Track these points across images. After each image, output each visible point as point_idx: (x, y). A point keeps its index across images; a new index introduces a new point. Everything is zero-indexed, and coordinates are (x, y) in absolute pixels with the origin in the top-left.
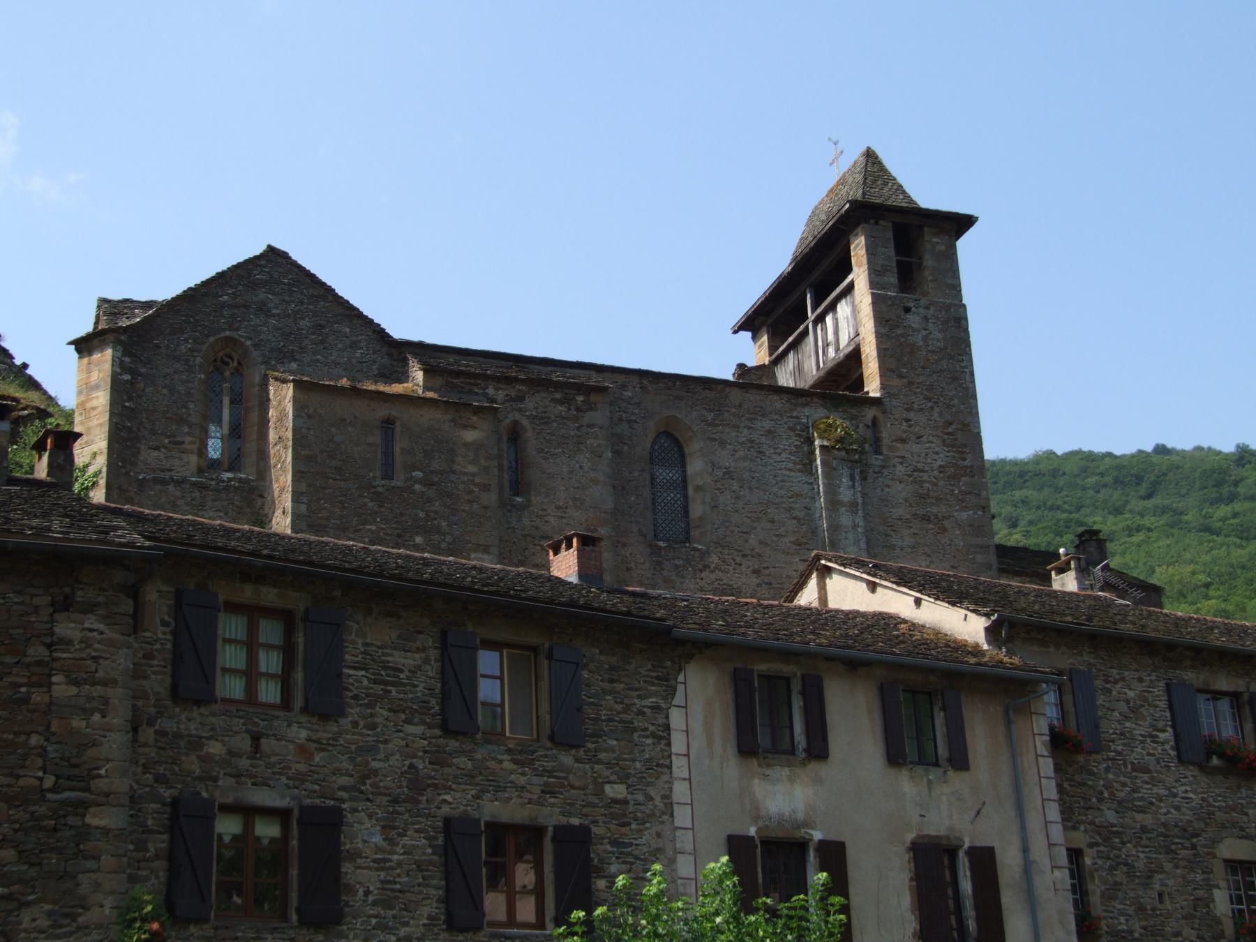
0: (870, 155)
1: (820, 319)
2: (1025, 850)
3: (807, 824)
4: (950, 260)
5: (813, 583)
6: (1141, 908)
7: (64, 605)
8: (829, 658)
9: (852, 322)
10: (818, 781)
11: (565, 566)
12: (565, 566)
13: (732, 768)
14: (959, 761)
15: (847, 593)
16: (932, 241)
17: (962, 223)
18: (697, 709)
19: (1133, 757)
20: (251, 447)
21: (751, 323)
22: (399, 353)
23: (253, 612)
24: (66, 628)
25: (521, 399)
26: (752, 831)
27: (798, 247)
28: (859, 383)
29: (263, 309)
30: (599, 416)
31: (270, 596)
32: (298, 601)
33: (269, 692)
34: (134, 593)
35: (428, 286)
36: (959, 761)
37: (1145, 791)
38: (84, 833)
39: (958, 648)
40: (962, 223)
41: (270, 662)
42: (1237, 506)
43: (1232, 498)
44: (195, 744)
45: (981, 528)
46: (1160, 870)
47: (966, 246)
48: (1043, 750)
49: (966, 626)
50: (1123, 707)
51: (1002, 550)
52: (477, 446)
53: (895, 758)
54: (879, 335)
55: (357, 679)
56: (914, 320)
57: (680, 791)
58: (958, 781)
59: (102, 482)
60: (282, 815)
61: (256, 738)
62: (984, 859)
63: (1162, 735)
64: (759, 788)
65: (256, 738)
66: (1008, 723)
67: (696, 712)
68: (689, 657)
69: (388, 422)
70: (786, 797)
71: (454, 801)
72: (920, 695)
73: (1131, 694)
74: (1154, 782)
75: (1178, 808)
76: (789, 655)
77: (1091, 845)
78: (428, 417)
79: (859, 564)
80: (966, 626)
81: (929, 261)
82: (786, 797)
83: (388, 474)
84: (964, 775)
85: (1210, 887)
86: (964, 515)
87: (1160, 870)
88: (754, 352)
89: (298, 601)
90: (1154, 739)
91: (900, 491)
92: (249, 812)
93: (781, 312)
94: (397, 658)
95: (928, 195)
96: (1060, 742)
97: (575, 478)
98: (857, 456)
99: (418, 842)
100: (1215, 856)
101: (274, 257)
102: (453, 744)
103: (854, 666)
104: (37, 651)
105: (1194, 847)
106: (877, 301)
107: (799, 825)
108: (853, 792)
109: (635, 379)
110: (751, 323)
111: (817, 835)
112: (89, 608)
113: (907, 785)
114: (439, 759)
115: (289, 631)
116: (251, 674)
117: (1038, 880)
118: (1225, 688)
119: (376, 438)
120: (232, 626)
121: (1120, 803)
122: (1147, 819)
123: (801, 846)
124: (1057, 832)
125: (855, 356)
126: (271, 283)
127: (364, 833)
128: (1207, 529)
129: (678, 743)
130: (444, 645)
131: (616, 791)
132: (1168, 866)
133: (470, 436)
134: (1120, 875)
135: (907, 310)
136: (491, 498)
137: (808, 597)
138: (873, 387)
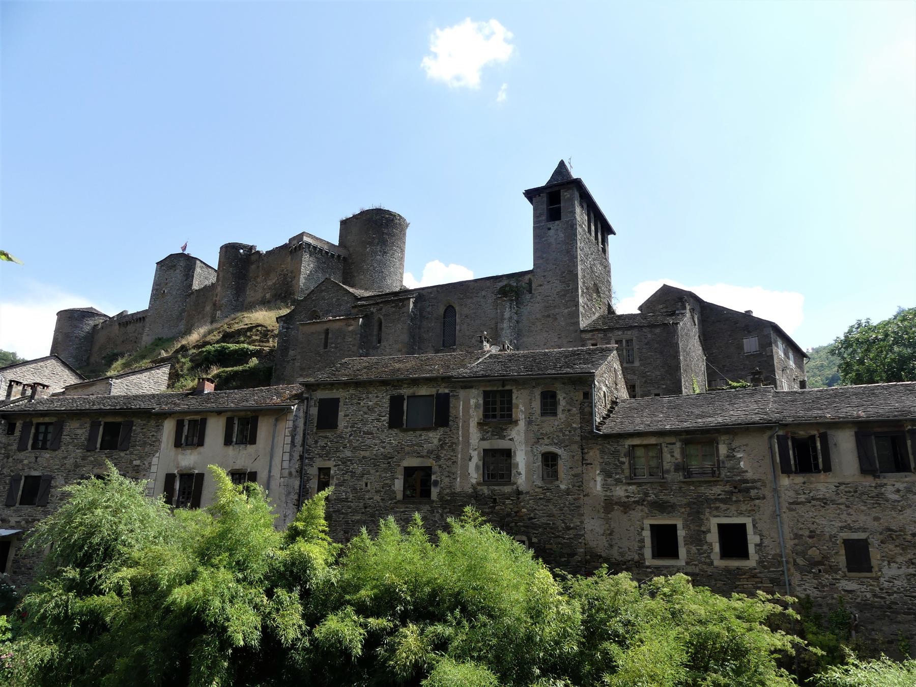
2: (270, 472)
3: (194, 468)
6: (355, 489)
10: (200, 453)
19: (365, 429)
25: (381, 309)
26: (176, 472)
29: (324, 299)
37: (368, 442)
44: (21, 461)
48: (287, 433)
50: (365, 409)
55: (66, 438)
56: (552, 232)
58: (251, 448)
61: (37, 458)
63: (383, 418)
64: (180, 457)
65: (37, 458)
66: (275, 425)
68: (166, 418)
70: (189, 460)
73: (370, 403)
74: (374, 438)
75: (384, 448)
77: (335, 466)
82: (189, 460)
84: (254, 446)
85: (393, 478)
86: (566, 311)
90: (378, 420)
100: (399, 466)
102: (89, 453)
105: (389, 463)
107: (191, 469)
109: (488, 283)
111: (196, 472)
118: (424, 394)
121: (354, 448)
122: (367, 454)
124: (286, 464)
132: (372, 471)
134: (347, 477)
135: (549, 229)
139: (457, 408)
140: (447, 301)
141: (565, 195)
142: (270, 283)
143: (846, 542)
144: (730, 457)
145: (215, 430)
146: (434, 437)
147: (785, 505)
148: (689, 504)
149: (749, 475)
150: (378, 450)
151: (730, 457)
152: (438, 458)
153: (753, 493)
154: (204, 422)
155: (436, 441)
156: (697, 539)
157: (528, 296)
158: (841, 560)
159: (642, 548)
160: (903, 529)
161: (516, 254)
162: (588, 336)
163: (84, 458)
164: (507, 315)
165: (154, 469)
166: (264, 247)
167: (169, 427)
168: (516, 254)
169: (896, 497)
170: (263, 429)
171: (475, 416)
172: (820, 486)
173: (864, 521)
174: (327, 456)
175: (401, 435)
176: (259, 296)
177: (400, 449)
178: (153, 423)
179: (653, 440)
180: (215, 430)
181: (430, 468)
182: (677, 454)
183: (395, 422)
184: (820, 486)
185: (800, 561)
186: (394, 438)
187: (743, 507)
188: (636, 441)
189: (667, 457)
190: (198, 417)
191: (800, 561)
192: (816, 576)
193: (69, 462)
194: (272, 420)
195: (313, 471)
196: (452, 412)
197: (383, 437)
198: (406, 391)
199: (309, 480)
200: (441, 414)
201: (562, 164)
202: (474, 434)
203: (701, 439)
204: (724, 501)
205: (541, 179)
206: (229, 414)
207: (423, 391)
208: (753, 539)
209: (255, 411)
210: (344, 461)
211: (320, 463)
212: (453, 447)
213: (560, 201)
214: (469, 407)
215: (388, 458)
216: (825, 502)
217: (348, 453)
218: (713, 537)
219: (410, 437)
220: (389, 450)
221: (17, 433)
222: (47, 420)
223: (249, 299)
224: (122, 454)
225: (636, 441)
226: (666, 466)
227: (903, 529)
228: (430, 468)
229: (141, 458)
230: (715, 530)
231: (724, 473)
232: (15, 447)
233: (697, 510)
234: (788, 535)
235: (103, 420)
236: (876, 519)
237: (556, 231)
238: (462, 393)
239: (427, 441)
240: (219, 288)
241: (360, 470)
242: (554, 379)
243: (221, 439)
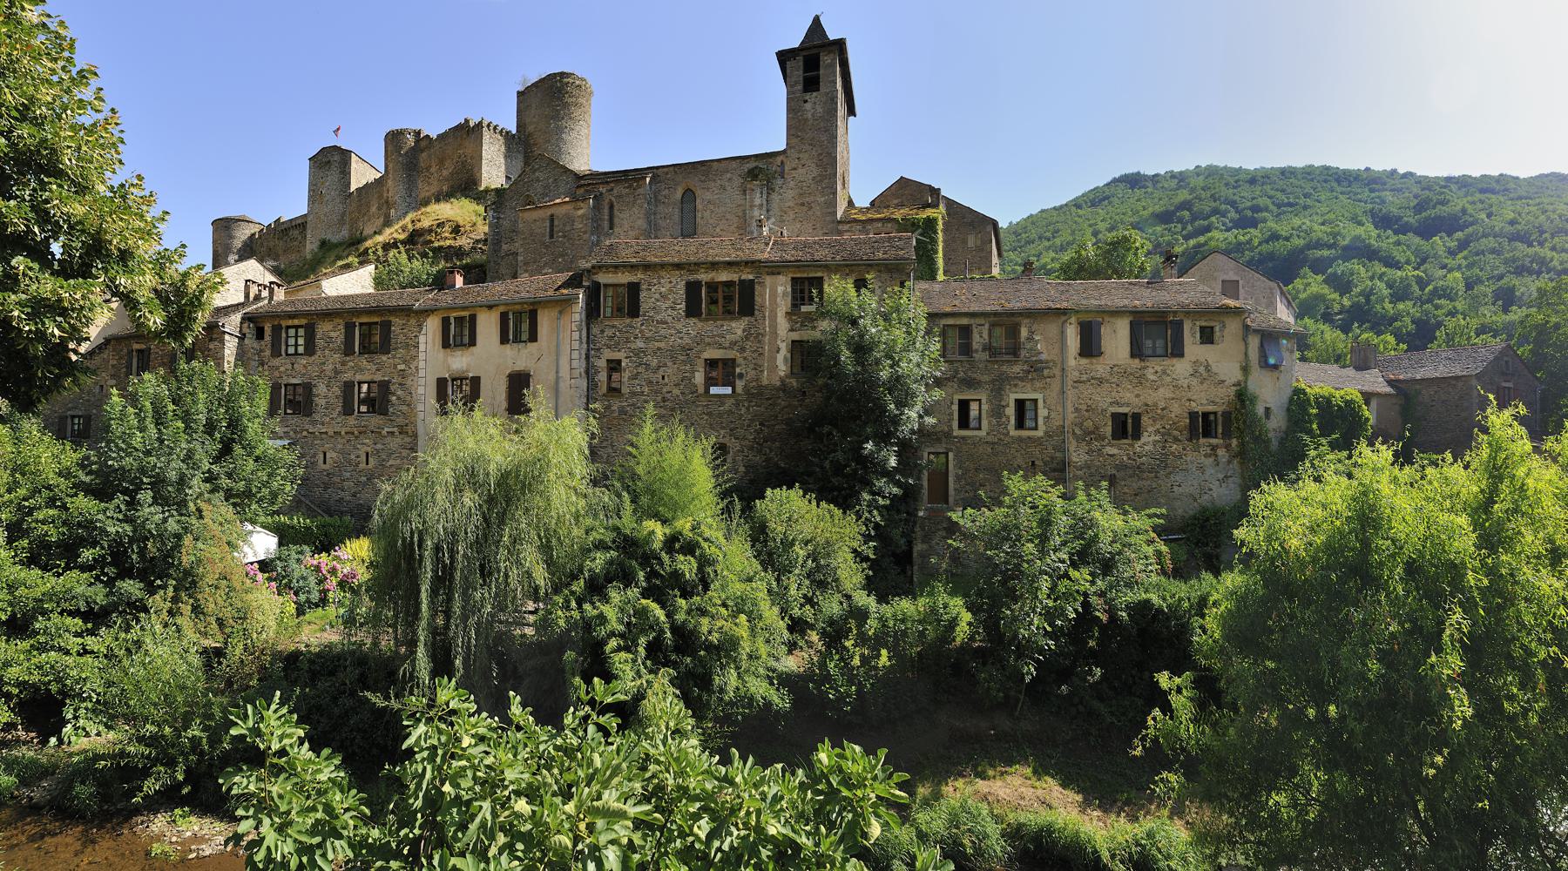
18: (430, 336)
19: (658, 318)
33: (301, 350)
37: (663, 332)
41: (301, 341)
46: (665, 365)
52: (582, 216)
55: (320, 343)
56: (808, 106)
57: (422, 365)
58: (532, 346)
64: (450, 360)
70: (460, 362)
71: (347, 376)
82: (460, 362)
85: (693, 372)
87: (665, 365)
99: (337, 391)
109: (734, 164)
113: (509, 350)
114: (343, 364)
117: (562, 385)
122: (662, 345)
127: (321, 389)
129: (422, 347)
131: (402, 367)
133: (580, 212)
139: (763, 296)
140: (677, 188)
141: (825, 59)
142: (445, 173)
143: (1114, 415)
144: (1030, 339)
145: (488, 326)
146: (738, 327)
147: (1070, 383)
148: (993, 381)
149: (1044, 357)
150: (675, 341)
151: (1030, 339)
152: (743, 349)
153: (1046, 372)
154: (473, 319)
155: (739, 332)
156: (998, 412)
157: (779, 182)
158: (1108, 430)
159: (950, 420)
160: (1156, 405)
161: (766, 130)
162: (846, 227)
163: (343, 364)
164: (758, 201)
165: (422, 373)
166: (433, 130)
167: (432, 325)
168: (766, 130)
169: (1152, 377)
170: (545, 321)
171: (784, 305)
172: (1099, 367)
173: (1129, 399)
174: (616, 347)
175: (700, 325)
176: (434, 189)
177: (699, 341)
178: (413, 321)
179: (965, 321)
180: (488, 326)
181: (734, 360)
182: (985, 335)
183: (693, 310)
184: (1099, 367)
185: (1078, 432)
186: (693, 327)
187: (1038, 385)
188: (950, 321)
189: (976, 337)
190: (466, 314)
191: (1078, 432)
192: (1089, 443)
193: (329, 367)
194: (554, 313)
195: (601, 364)
196: (758, 299)
197: (679, 326)
198: (704, 277)
199: (597, 372)
200: (741, 300)
201: (817, 21)
202: (783, 324)
203: (1008, 322)
204: (1022, 379)
205: (795, 41)
206: (502, 309)
207: (724, 277)
208: (1042, 412)
209: (533, 304)
210: (638, 353)
211: (608, 354)
212: (759, 337)
213: (815, 66)
214: (776, 293)
215: (686, 349)
216: (1101, 381)
217: (640, 344)
218: (1011, 411)
219: (709, 327)
220: (687, 340)
221: (267, 338)
222: (296, 322)
223: (422, 195)
224: (384, 358)
225: (950, 321)
226: (975, 346)
227: (1156, 405)
228: (734, 360)
229: (405, 362)
230: (1012, 404)
231: (1023, 353)
232: (268, 353)
233: (998, 389)
234: (1070, 409)
235: (358, 321)
236: (1138, 396)
237: (813, 105)
238: (768, 280)
239: (730, 331)
240: (390, 182)
241: (654, 363)
242: (870, 266)
243: (496, 337)
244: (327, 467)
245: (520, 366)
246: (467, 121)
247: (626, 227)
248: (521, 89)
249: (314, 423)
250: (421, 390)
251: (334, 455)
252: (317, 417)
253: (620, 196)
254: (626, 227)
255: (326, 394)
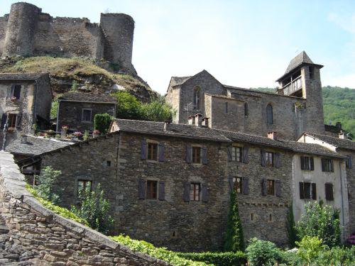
0: (304, 53)
1: (294, 82)
4: (318, 73)
5: (303, 137)
7: (220, 149)
8: (315, 155)
9: (301, 83)
11: (271, 136)
12: (271, 136)
13: (300, 171)
14: (332, 171)
15: (309, 140)
16: (316, 70)
17: (321, 66)
20: (201, 105)
21: (279, 81)
22: (225, 89)
23: (236, 147)
24: (220, 152)
27: (288, 69)
28: (302, 95)
30: (260, 102)
31: (239, 145)
32: (242, 146)
33: (238, 160)
34: (17, 94)
35: (230, 77)
36: (332, 171)
38: (223, 182)
39: (331, 151)
40: (321, 66)
42: (345, 100)
43: (343, 99)
45: (322, 123)
47: (321, 70)
49: (333, 148)
51: (326, 126)
53: (324, 170)
54: (306, 84)
56: (312, 84)
59: (178, 114)
60: (241, 178)
62: (314, 185)
64: (304, 175)
67: (296, 161)
69: (227, 103)
71: (264, 176)
72: (327, 160)
76: (308, 154)
78: (233, 102)
79: (312, 135)
80: (333, 148)
81: (315, 74)
82: (308, 176)
83: (227, 112)
88: (280, 86)
89: (242, 146)
91: (309, 116)
92: (236, 177)
93: (286, 80)
94: (255, 154)
95: (315, 62)
96: (347, 167)
97: (256, 113)
98: (303, 109)
99: (258, 183)
101: (205, 72)
103: (318, 156)
104: (217, 156)
106: (306, 81)
108: (317, 176)
110: (279, 81)
112: (223, 149)
113: (325, 174)
115: (241, 150)
116: (236, 157)
119: (225, 106)
120: (267, 154)
123: (310, 184)
125: (301, 90)
126: (204, 75)
127: (251, 181)
128: (338, 105)
129: (293, 168)
130: (261, 152)
131: (284, 175)
133: (240, 106)
136: (243, 117)
137: (301, 140)
138: (304, 96)
193: (254, 171)
244: (253, 222)
245: (329, 181)
246: (117, 31)
247: (253, 116)
248: (104, 13)
249: (248, 198)
250: (293, 187)
251: (257, 216)
252: (250, 195)
253: (250, 102)
254: (253, 116)
255: (253, 184)
